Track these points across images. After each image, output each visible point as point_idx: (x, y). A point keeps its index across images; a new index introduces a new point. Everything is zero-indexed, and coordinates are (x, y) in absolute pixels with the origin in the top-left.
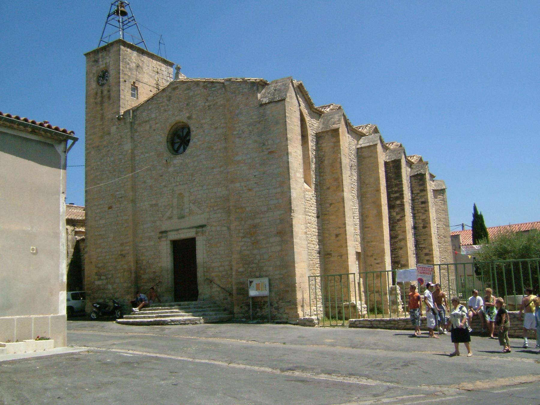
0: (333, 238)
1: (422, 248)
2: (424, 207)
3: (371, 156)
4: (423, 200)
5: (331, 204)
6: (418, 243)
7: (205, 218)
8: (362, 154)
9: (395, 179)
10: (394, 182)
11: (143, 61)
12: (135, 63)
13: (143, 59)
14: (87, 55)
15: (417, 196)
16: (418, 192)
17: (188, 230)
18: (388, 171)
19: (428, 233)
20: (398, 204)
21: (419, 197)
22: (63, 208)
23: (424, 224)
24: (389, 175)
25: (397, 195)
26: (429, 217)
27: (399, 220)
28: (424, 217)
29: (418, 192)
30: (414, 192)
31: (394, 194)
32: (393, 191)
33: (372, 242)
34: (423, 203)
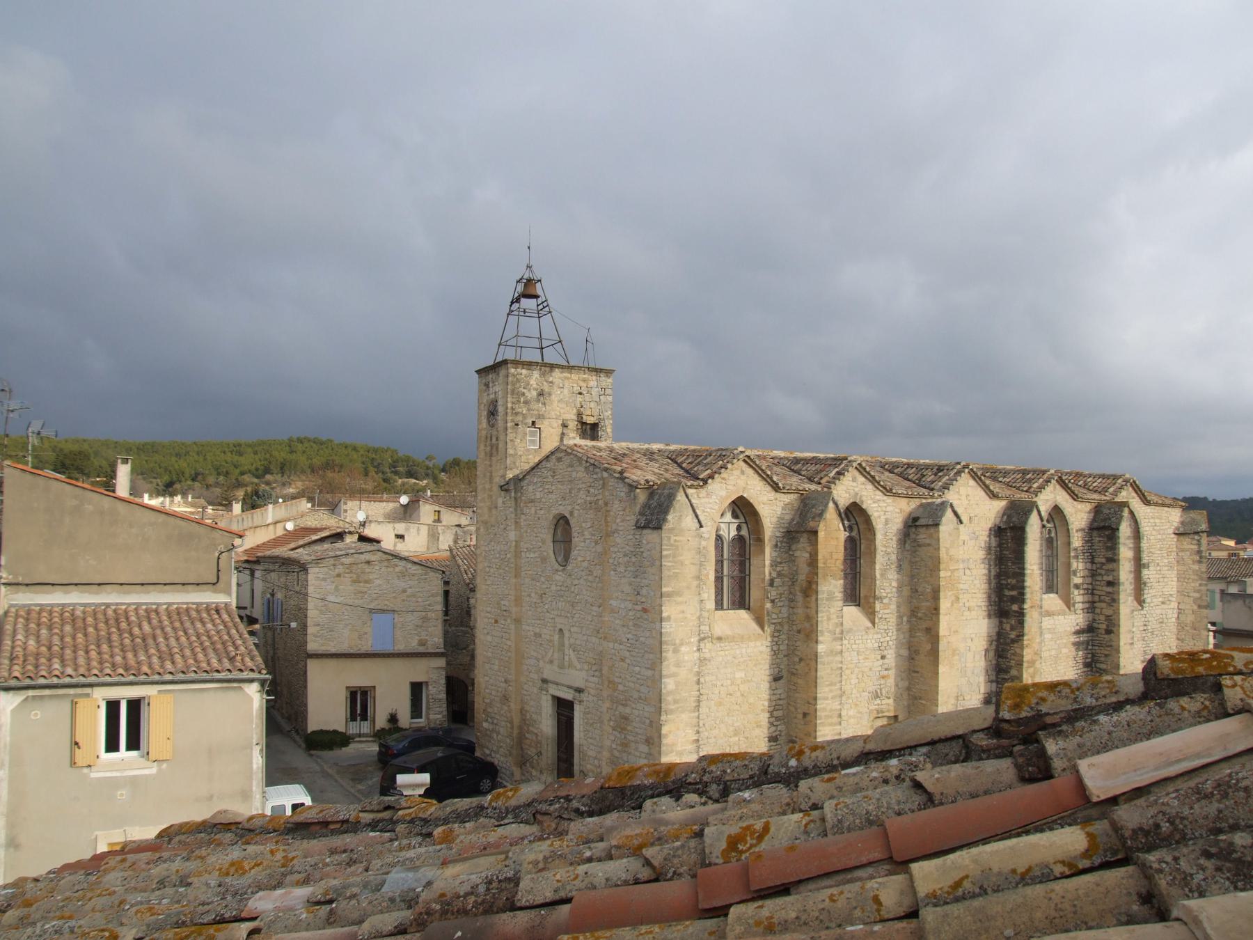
0: (800, 716)
1: (1100, 669)
2: (1110, 593)
3: (929, 545)
4: (1110, 578)
5: (801, 660)
6: (1095, 658)
8: (918, 537)
9: (1013, 563)
10: (1012, 568)
11: (551, 382)
12: (536, 389)
13: (551, 379)
14: (478, 372)
15: (1101, 568)
16: (1103, 560)
17: (565, 689)
18: (1003, 544)
19: (1113, 644)
20: (1015, 612)
21: (1103, 572)
22: (257, 764)
23: (1107, 626)
24: (1005, 552)
25: (1014, 593)
26: (1117, 613)
27: (1013, 641)
28: (1108, 612)
29: (1103, 560)
30: (1097, 560)
31: (1009, 590)
32: (1008, 584)
33: (920, 698)
34: (1110, 584)
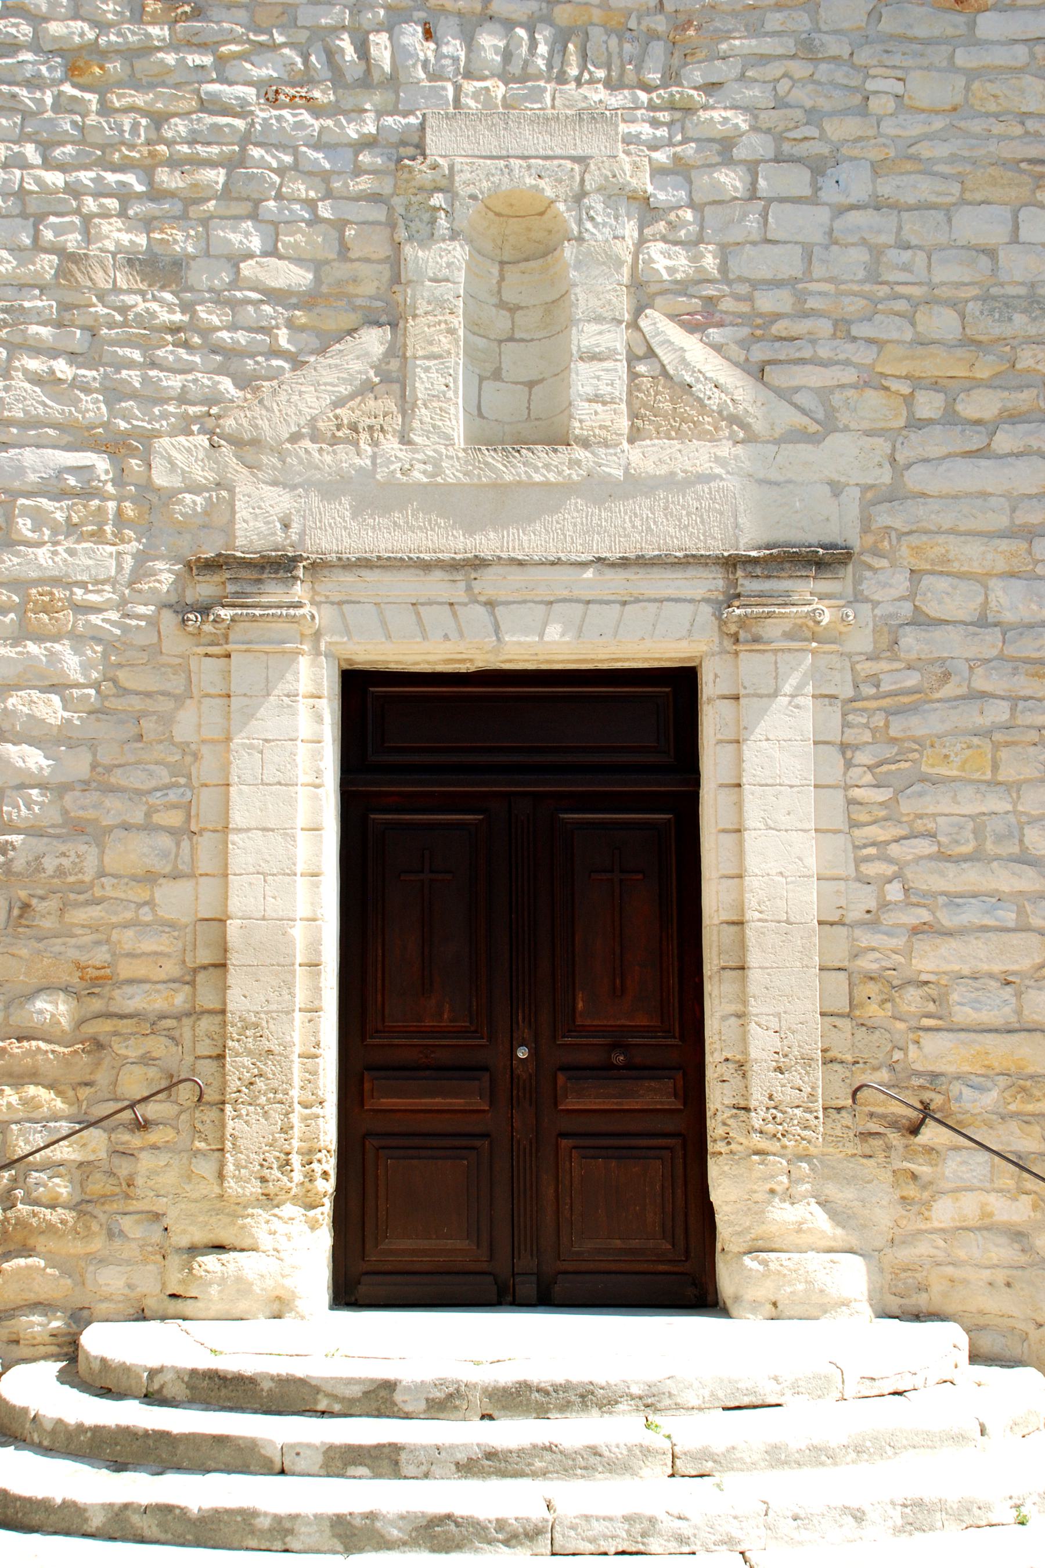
7: (836, 489)
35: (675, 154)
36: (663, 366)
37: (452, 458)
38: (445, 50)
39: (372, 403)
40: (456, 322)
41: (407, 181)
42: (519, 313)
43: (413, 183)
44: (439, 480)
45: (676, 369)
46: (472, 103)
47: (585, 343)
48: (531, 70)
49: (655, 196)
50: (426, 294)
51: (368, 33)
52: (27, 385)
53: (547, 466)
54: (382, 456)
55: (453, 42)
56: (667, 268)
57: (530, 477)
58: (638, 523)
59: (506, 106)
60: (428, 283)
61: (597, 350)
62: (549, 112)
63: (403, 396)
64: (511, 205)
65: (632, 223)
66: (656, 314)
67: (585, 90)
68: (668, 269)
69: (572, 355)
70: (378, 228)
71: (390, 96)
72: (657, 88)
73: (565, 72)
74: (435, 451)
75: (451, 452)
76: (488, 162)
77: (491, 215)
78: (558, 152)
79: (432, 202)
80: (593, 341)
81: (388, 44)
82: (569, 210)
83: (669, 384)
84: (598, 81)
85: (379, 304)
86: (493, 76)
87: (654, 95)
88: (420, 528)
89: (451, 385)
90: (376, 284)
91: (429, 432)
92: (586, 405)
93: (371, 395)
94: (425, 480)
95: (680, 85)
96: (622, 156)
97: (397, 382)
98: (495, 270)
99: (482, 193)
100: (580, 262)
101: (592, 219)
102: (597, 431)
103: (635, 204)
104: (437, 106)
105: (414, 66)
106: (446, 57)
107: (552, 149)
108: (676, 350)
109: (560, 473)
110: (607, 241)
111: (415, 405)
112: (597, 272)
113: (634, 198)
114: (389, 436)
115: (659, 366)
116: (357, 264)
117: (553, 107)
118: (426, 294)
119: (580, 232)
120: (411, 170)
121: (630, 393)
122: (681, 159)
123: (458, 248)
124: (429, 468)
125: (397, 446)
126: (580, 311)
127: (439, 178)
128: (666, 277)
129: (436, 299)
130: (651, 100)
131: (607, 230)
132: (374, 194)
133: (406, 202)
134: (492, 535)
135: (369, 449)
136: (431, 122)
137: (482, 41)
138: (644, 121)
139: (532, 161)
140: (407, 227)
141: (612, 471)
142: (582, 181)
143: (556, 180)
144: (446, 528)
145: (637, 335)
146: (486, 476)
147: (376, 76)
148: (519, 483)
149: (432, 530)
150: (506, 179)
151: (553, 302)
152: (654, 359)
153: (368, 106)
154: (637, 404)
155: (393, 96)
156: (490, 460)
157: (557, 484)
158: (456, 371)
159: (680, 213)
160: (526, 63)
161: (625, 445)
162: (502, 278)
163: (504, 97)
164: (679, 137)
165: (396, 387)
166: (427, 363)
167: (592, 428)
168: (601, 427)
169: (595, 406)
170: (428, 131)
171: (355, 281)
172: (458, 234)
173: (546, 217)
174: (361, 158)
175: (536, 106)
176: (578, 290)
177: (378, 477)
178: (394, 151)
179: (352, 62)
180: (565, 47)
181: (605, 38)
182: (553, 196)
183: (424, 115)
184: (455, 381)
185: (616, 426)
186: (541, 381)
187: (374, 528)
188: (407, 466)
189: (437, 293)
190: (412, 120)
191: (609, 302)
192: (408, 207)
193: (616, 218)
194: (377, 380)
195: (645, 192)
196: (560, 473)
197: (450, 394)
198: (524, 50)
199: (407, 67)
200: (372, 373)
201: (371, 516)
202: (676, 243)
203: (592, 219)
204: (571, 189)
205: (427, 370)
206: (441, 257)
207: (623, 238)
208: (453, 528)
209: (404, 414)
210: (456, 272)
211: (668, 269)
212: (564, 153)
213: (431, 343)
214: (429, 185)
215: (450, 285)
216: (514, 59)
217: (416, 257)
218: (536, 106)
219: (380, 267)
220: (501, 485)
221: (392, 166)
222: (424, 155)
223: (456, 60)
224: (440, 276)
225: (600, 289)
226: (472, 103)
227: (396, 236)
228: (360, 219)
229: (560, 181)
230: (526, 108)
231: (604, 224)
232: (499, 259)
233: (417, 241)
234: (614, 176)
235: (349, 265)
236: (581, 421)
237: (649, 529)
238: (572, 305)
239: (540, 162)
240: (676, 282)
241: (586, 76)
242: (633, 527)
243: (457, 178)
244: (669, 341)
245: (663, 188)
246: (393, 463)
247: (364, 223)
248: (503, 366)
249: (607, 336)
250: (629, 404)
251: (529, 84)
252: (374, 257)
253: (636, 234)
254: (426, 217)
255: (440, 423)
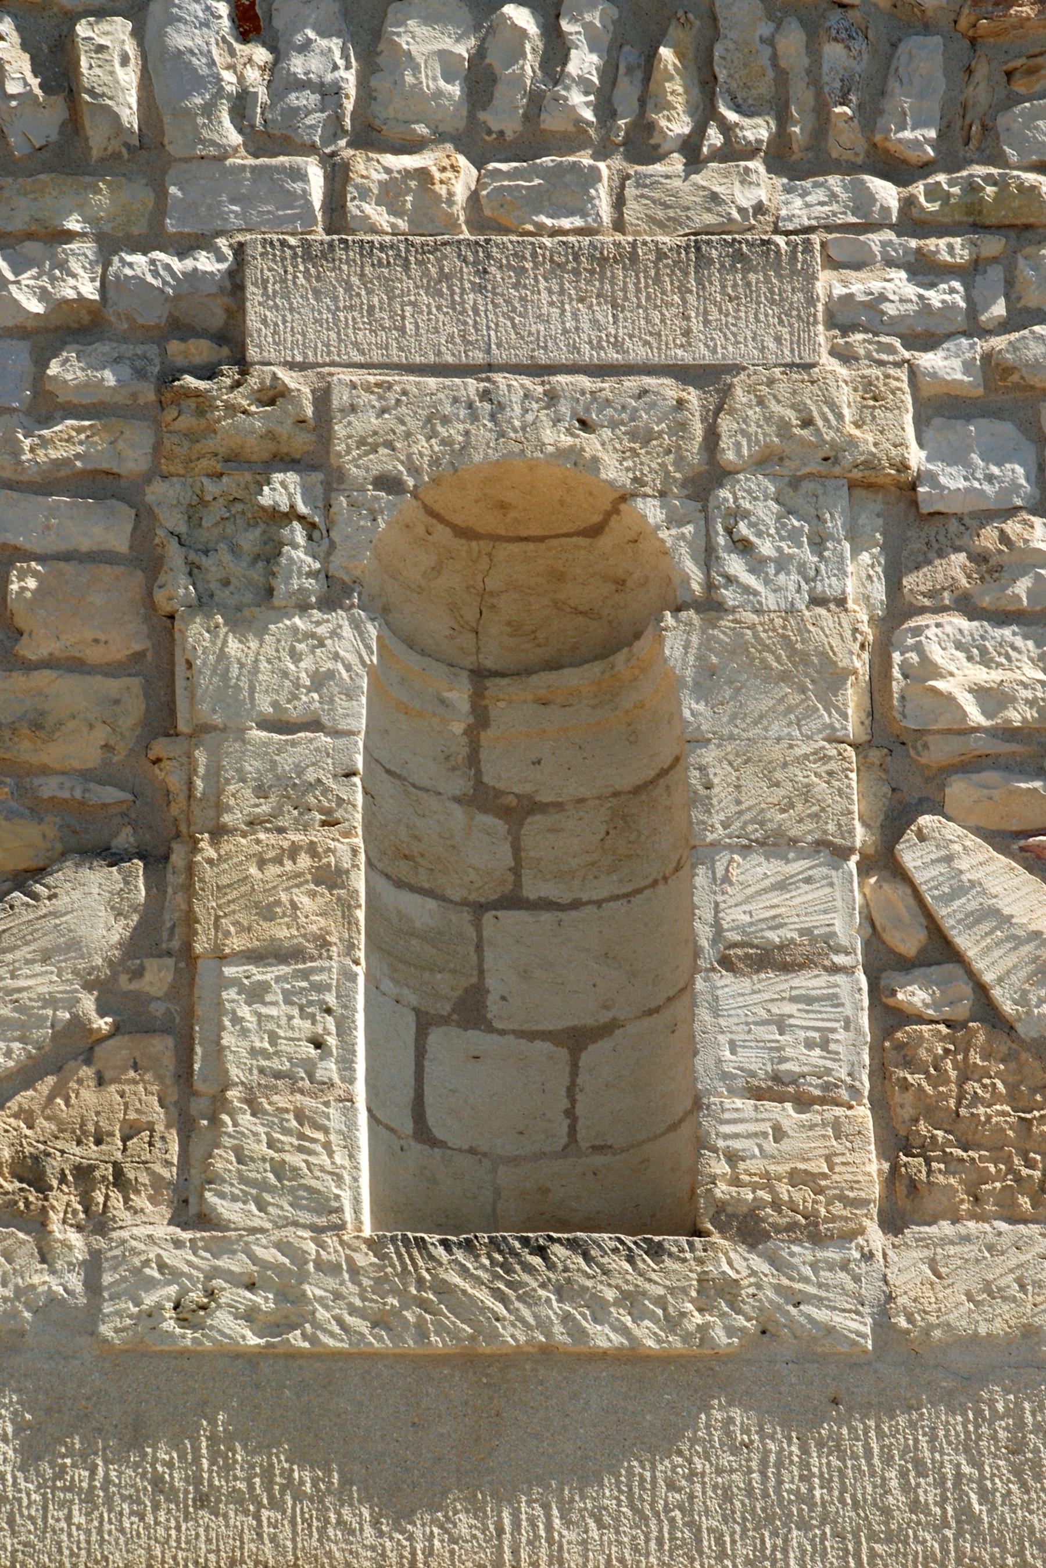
35: (987, 357)
36: (981, 989)
37: (334, 1269)
38: (298, 65)
39: (88, 1096)
40: (342, 848)
41: (192, 437)
42: (537, 821)
43: (211, 444)
44: (296, 1339)
45: (1023, 1000)
46: (379, 216)
47: (735, 916)
48: (550, 122)
49: (932, 478)
50: (252, 766)
51: (73, 18)
52: (263, 734)
53: (631, 1300)
54: (118, 1262)
55: (324, 43)
56: (980, 693)
57: (578, 1333)
58: (929, 1495)
59: (478, 220)
60: (258, 734)
61: (774, 936)
62: (608, 239)
63: (184, 1074)
64: (503, 506)
65: (865, 557)
66: (952, 830)
67: (710, 177)
68: (981, 693)
69: (697, 952)
70: (107, 572)
71: (142, 196)
72: (926, 168)
73: (651, 127)
74: (282, 1246)
75: (334, 1250)
76: (432, 382)
77: (442, 534)
78: (638, 353)
79: (267, 497)
80: (760, 909)
81: (131, 47)
82: (673, 520)
83: (1003, 1047)
84: (751, 152)
85: (111, 794)
86: (440, 137)
87: (918, 189)
88: (236, 1498)
89: (332, 1041)
90: (101, 734)
91: (263, 1186)
92: (745, 1105)
93: (86, 1072)
94: (253, 1340)
95: (997, 159)
96: (829, 363)
97: (166, 1030)
98: (460, 696)
99: (415, 471)
100: (713, 672)
101: (743, 547)
102: (784, 1190)
103: (875, 504)
104: (277, 223)
105: (209, 110)
106: (301, 85)
107: (618, 346)
108: (1018, 942)
109: (673, 1323)
110: (791, 610)
111: (219, 1103)
112: (766, 704)
113: (870, 486)
114: (140, 1201)
115: (967, 989)
116: (42, 678)
117: (619, 225)
118: (252, 766)
119: (710, 586)
120: (202, 403)
121: (880, 1072)
122: (1008, 371)
123: (347, 631)
124: (264, 1301)
125: (163, 1230)
126: (716, 819)
127: (284, 430)
128: (975, 716)
129: (283, 782)
130: (907, 203)
131: (790, 580)
132: (94, 474)
133: (188, 497)
134: (464, 1523)
135: (75, 1238)
136: (259, 267)
137: (404, 42)
138: (890, 263)
139: (562, 379)
140: (193, 570)
141: (838, 1320)
142: (712, 436)
143: (633, 436)
144: (318, 1498)
145: (896, 894)
146: (441, 1329)
147: (97, 138)
148: (547, 1353)
149: (275, 1504)
150: (483, 432)
151: (637, 790)
152: (951, 968)
153: (73, 224)
154: (904, 1106)
155: (146, 197)
156: (454, 1278)
157: (666, 1360)
158: (348, 1005)
159: (1012, 527)
160: (536, 101)
161: (876, 1237)
162: (481, 718)
163: (474, 198)
164: (999, 309)
165: (162, 1046)
166: (259, 974)
167: (768, 1181)
168: (796, 1178)
169: (773, 1109)
170: (252, 292)
171: (37, 726)
172: (347, 591)
173: (605, 542)
174: (54, 369)
175: (566, 223)
176: (709, 755)
177: (105, 1330)
178: (152, 350)
179: (27, 96)
180: (651, 57)
181: (766, 29)
182: (625, 479)
183: (239, 250)
184: (344, 1029)
185: (841, 1176)
186: (607, 1029)
187: (89, 1498)
188: (197, 1296)
189: (286, 762)
190: (205, 263)
191: (806, 793)
192: (194, 511)
193: (818, 544)
194: (103, 1024)
195: (903, 467)
196: (673, 1323)
197: (329, 1069)
198: (530, 65)
199: (189, 114)
200: (88, 1003)
201: (84, 1458)
202: (1001, 618)
203: (743, 547)
204: (678, 463)
205: (256, 994)
206: (296, 657)
207: (841, 602)
208: (343, 1498)
209: (186, 1128)
210: (340, 702)
211: (981, 693)
212: (655, 358)
213: (268, 913)
214: (257, 450)
215: (324, 739)
216: (500, 91)
217: (222, 656)
218: (566, 223)
219: (113, 686)
220: (492, 1359)
221: (148, 394)
222: (243, 365)
223: (330, 93)
224: (294, 712)
225: (777, 753)
226: (379, 216)
227: (160, 596)
228: (52, 544)
229: (646, 437)
230: (541, 230)
231: (782, 563)
232: (469, 661)
233: (223, 609)
234: (807, 422)
235: (19, 680)
236: (733, 1158)
237: (965, 1513)
238: (693, 800)
239: (584, 381)
240: (1008, 733)
241: (714, 137)
242: (915, 1506)
243: (340, 430)
244: (994, 913)
245: (956, 457)
246: (151, 1284)
247: (66, 557)
248: (490, 982)
249: (804, 895)
250: (880, 1105)
251: (547, 161)
252: (95, 655)
253: (879, 591)
254: (250, 540)
255: (296, 1160)
